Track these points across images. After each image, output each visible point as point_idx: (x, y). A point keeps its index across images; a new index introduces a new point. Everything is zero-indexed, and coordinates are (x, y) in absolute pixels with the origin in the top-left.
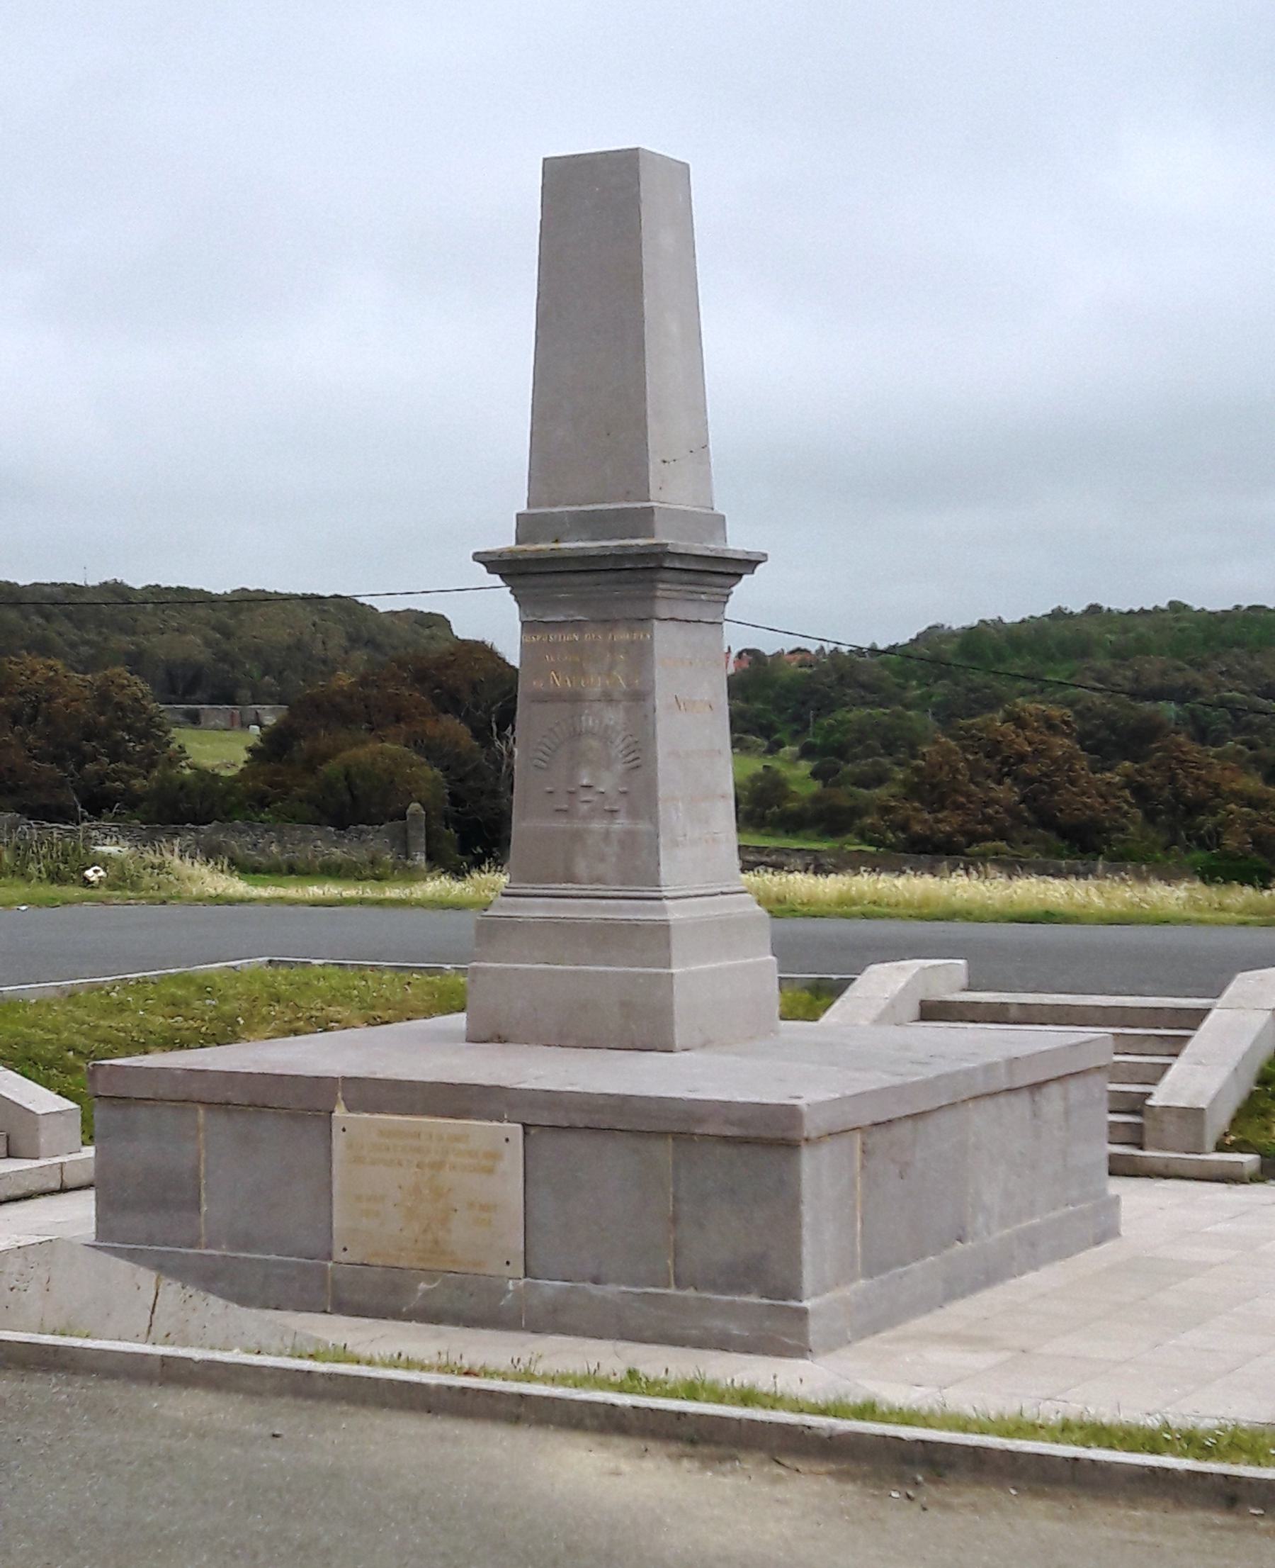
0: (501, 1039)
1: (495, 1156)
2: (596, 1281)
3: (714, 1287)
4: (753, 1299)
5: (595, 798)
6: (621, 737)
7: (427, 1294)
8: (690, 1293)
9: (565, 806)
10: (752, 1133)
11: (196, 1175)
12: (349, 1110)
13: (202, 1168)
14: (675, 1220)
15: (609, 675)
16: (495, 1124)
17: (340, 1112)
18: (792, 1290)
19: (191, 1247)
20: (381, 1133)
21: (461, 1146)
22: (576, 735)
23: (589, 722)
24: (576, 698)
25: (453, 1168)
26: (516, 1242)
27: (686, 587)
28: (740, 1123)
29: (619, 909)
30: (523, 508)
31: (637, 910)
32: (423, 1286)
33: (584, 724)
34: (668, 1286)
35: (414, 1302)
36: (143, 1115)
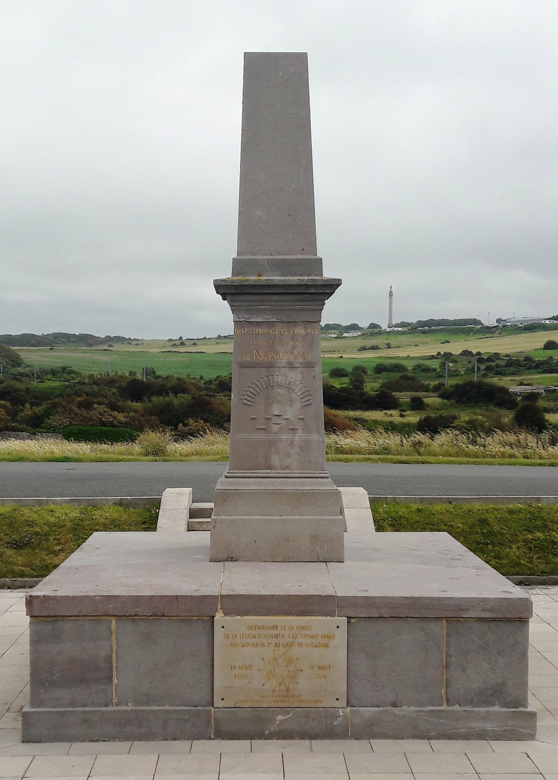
0: (232, 559)
1: (330, 637)
2: (394, 705)
3: (471, 703)
4: (497, 708)
5: (283, 422)
6: (299, 388)
7: (282, 722)
8: (456, 708)
9: (264, 427)
10: (500, 615)
11: (109, 658)
12: (226, 614)
13: (114, 655)
14: (447, 666)
15: (292, 353)
16: (328, 618)
17: (219, 616)
18: (522, 702)
19: (106, 706)
20: (250, 628)
21: (307, 632)
22: (270, 386)
23: (279, 379)
24: (270, 366)
25: (300, 645)
26: (343, 687)
27: (276, 303)
28: (492, 610)
29: (302, 484)
30: (235, 256)
32: (280, 717)
33: (275, 380)
34: (441, 705)
35: (272, 728)
36: (68, 626)
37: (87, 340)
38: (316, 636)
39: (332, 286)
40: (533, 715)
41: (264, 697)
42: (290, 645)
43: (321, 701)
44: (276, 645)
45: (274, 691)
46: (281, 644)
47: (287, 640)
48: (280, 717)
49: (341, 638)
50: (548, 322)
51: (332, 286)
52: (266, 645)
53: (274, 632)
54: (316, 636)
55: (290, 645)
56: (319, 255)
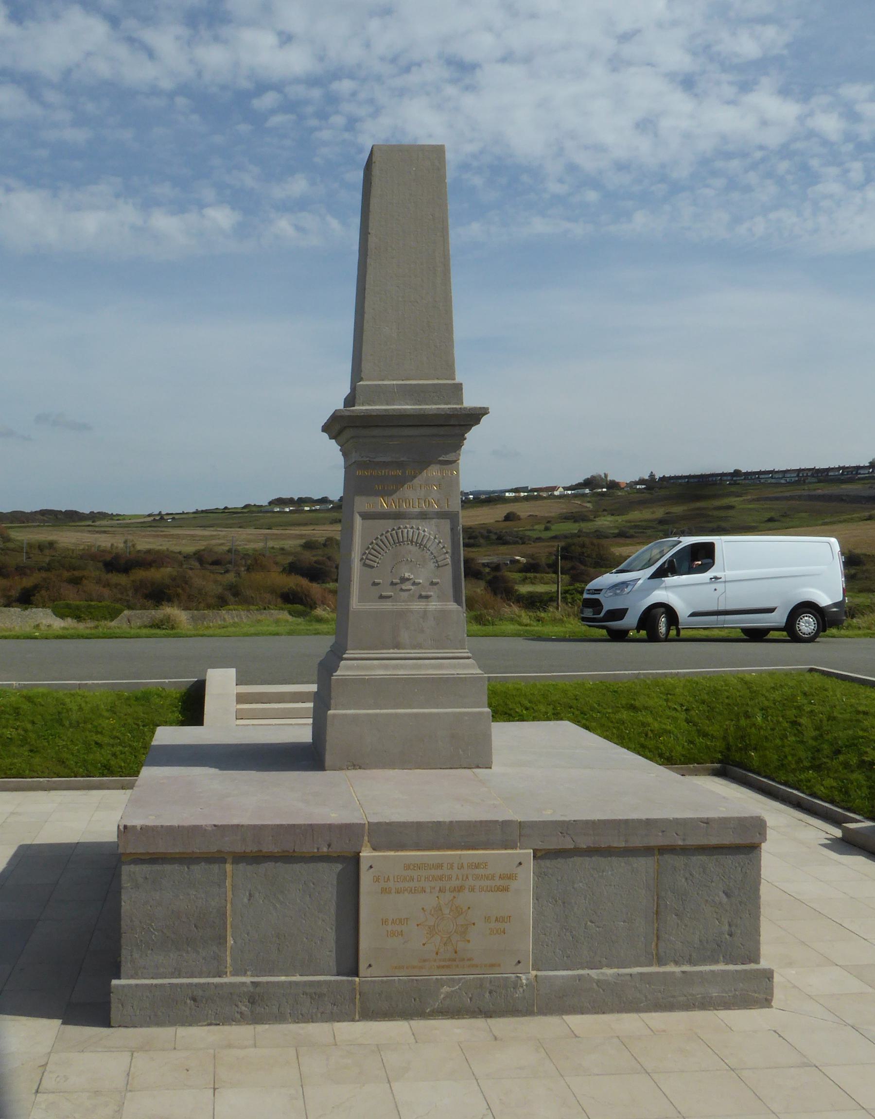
7: (448, 996)
17: (366, 853)
20: (407, 867)
25: (472, 889)
31: (454, 667)
37: (71, 518)
38: (493, 876)
39: (474, 417)
40: (768, 975)
41: (425, 961)
42: (460, 889)
43: (499, 965)
44: (440, 891)
45: (437, 954)
46: (448, 888)
47: (455, 883)
48: (445, 989)
49: (527, 876)
50: (507, 494)
51: (474, 417)
52: (428, 890)
53: (439, 872)
54: (493, 876)
55: (460, 889)
56: (458, 379)
